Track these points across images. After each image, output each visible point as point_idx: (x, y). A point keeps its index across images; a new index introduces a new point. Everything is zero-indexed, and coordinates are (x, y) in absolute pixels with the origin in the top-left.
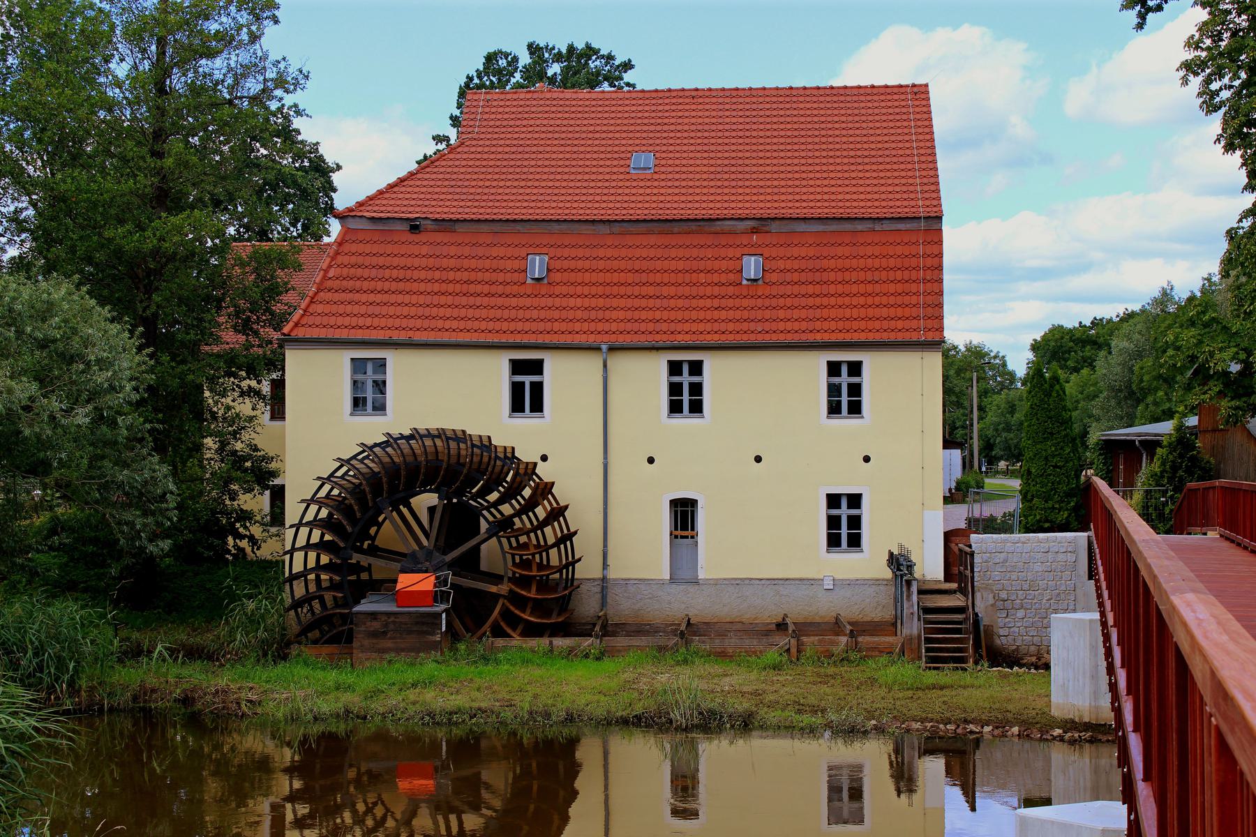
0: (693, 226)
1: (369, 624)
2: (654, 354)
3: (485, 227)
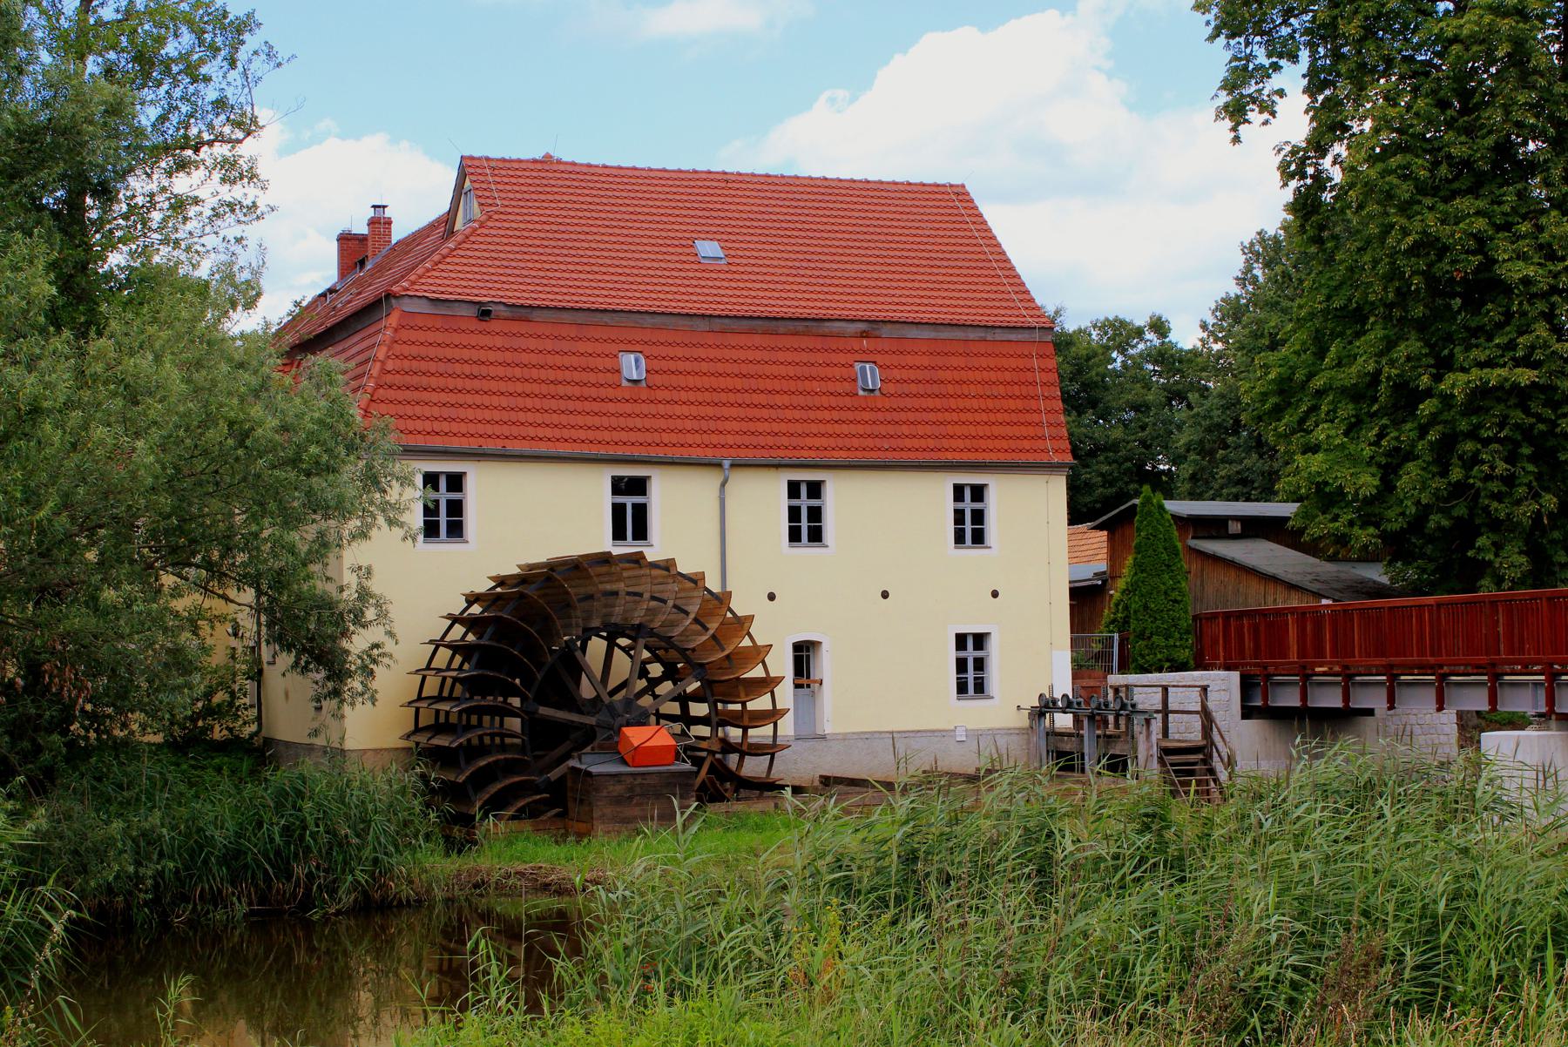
0: (800, 326)
1: (611, 788)
2: (771, 473)
3: (566, 316)
